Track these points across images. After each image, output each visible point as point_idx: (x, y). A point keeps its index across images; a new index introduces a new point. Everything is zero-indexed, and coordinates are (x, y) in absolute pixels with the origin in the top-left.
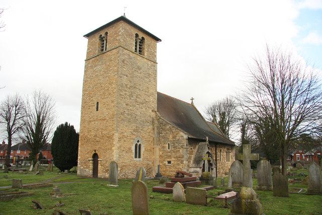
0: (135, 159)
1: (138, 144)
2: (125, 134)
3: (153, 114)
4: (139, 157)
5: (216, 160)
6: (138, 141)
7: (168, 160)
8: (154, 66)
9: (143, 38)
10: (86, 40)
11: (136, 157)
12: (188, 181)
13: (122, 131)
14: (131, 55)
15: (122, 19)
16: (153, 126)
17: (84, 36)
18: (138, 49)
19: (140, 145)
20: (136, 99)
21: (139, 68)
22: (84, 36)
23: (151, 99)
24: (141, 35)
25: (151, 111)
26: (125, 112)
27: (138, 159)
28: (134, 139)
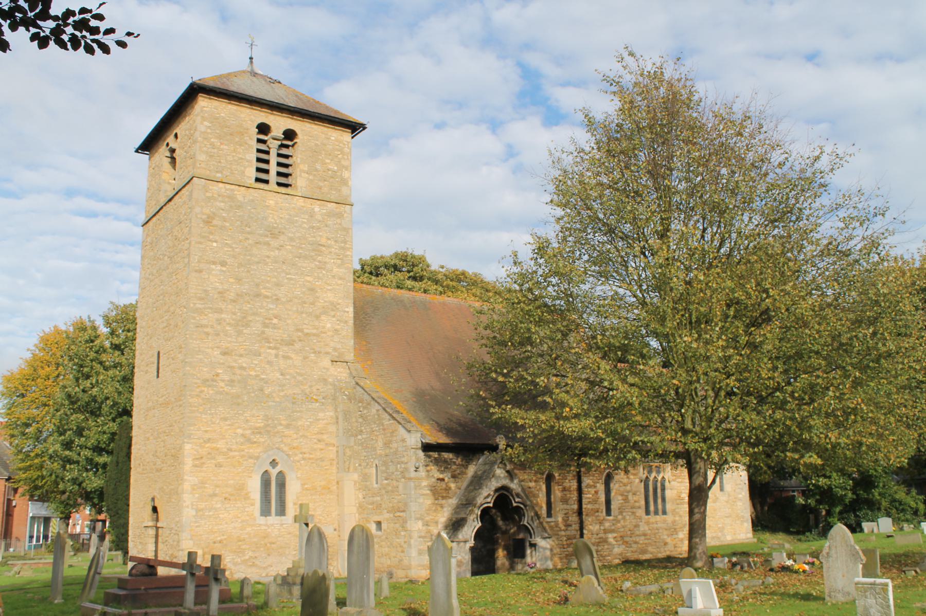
0: (262, 520)
1: (274, 472)
2: (221, 445)
3: (340, 373)
4: (282, 511)
5: (580, 512)
6: (274, 463)
7: (378, 518)
8: (340, 215)
9: (290, 135)
10: (144, 158)
11: (265, 512)
12: (156, 588)
13: (207, 436)
14: (240, 198)
15: (194, 92)
16: (336, 411)
17: (137, 151)
18: (273, 168)
19: (281, 475)
20: (263, 332)
21: (274, 233)
22: (137, 151)
23: (328, 323)
24: (279, 123)
25: (326, 362)
26: (217, 375)
27: (273, 519)
28: (257, 458)
